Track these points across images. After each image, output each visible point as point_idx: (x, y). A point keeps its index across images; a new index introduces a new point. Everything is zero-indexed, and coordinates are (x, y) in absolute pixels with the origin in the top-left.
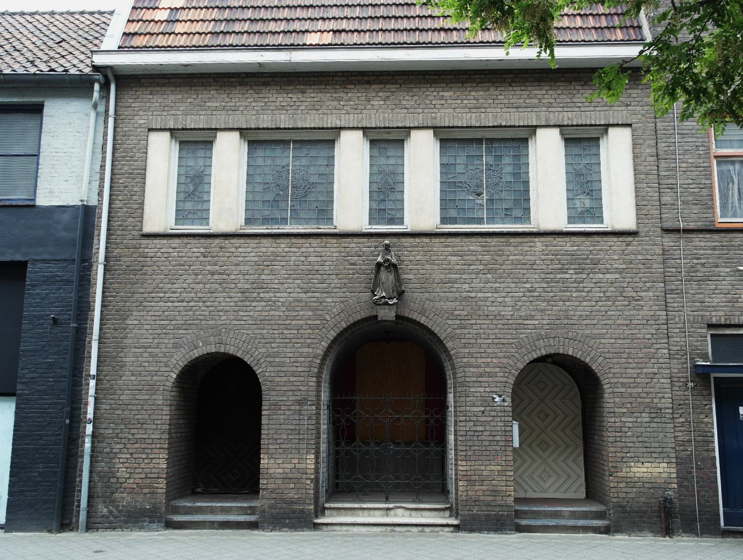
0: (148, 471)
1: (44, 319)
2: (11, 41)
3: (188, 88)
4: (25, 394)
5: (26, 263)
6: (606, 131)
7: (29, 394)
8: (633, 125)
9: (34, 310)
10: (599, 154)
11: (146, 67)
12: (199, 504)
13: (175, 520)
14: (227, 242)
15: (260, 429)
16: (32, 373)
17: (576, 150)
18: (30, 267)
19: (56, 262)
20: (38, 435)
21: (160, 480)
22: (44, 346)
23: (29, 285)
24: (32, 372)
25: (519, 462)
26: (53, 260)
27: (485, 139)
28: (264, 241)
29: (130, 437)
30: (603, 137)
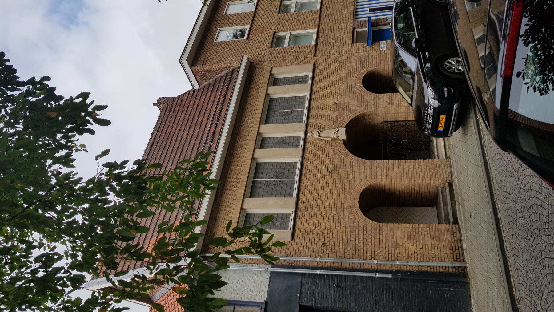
0: (426, 233)
1: (337, 294)
2: (166, 296)
3: (217, 221)
4: (384, 304)
5: (301, 306)
6: (244, 209)
7: (383, 301)
8: (272, 66)
9: (331, 300)
10: (265, 163)
11: (229, 128)
12: (443, 216)
13: (452, 221)
14: (301, 200)
15: (389, 93)
16: (370, 300)
17: (257, 193)
18: (304, 303)
19: (302, 287)
20: (409, 295)
21: (430, 227)
22: (353, 293)
23: (315, 304)
24: (369, 301)
25: (426, 222)
26: (301, 289)
27: (254, 179)
28: (302, 184)
29: (407, 243)
30: (247, 212)
